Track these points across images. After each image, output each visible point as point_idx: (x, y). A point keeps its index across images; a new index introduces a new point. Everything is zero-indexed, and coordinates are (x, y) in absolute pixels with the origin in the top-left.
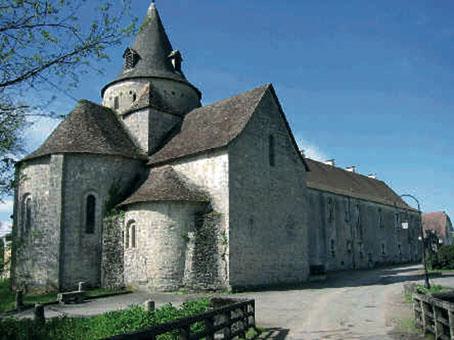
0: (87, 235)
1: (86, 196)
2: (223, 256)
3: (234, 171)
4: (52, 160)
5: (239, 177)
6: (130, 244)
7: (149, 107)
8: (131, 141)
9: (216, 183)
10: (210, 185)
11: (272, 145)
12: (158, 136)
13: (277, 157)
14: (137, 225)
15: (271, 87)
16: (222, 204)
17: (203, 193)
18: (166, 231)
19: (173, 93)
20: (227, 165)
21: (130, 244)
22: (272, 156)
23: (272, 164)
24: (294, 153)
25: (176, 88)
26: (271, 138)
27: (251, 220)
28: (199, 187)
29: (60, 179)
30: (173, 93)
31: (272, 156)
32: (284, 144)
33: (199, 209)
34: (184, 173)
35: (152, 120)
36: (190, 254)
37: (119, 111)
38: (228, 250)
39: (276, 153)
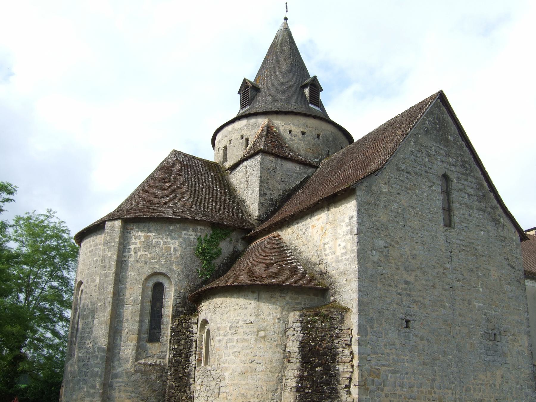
0: (149, 345)
1: (151, 284)
2: (348, 387)
3: (367, 233)
4: (107, 230)
5: (380, 243)
6: (203, 361)
7: (263, 152)
8: (237, 204)
9: (339, 251)
10: (329, 259)
11: (447, 192)
12: (275, 195)
13: (458, 215)
14: (211, 326)
15: (285, 51)
16: (348, 294)
17: (321, 273)
18: (252, 338)
19: (303, 133)
20: (355, 219)
21: (203, 361)
22: (448, 210)
23: (449, 224)
24: (494, 208)
25: (306, 126)
26: (446, 178)
27: (407, 322)
28: (315, 264)
29: (115, 257)
30: (303, 133)
31: (448, 210)
32: (470, 191)
33: (308, 290)
34: (296, 243)
35: (263, 170)
36: (79, 301)
37: (227, 165)
38: (356, 377)
39: (456, 205)
